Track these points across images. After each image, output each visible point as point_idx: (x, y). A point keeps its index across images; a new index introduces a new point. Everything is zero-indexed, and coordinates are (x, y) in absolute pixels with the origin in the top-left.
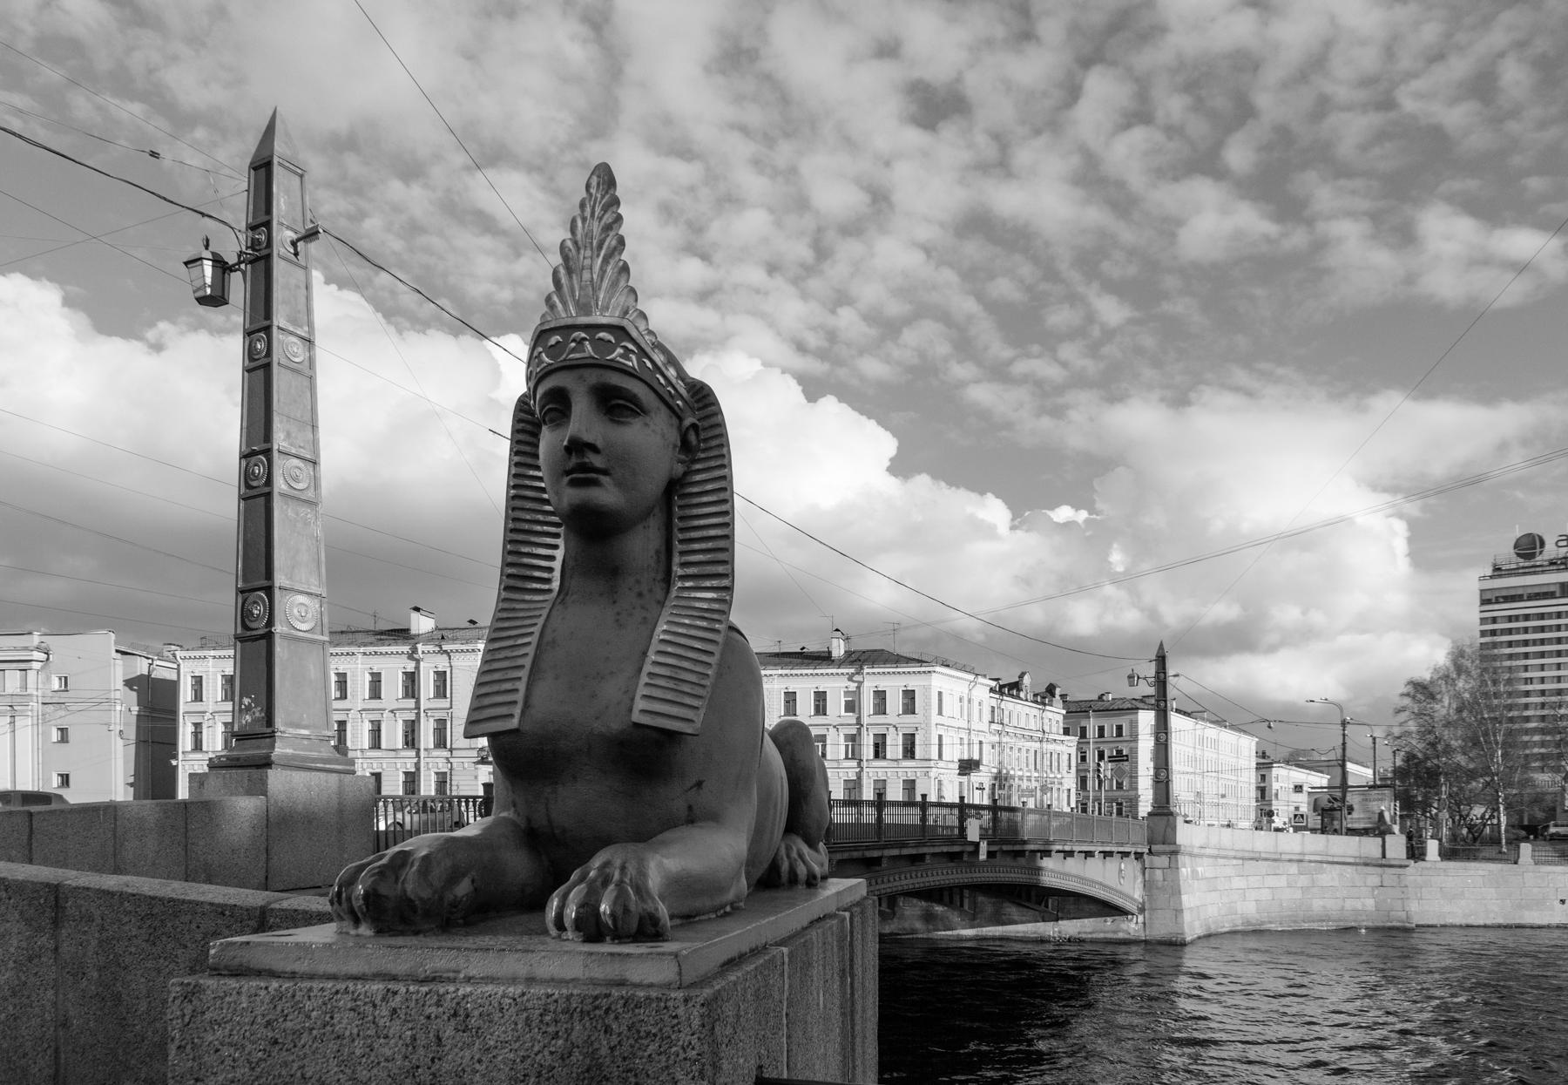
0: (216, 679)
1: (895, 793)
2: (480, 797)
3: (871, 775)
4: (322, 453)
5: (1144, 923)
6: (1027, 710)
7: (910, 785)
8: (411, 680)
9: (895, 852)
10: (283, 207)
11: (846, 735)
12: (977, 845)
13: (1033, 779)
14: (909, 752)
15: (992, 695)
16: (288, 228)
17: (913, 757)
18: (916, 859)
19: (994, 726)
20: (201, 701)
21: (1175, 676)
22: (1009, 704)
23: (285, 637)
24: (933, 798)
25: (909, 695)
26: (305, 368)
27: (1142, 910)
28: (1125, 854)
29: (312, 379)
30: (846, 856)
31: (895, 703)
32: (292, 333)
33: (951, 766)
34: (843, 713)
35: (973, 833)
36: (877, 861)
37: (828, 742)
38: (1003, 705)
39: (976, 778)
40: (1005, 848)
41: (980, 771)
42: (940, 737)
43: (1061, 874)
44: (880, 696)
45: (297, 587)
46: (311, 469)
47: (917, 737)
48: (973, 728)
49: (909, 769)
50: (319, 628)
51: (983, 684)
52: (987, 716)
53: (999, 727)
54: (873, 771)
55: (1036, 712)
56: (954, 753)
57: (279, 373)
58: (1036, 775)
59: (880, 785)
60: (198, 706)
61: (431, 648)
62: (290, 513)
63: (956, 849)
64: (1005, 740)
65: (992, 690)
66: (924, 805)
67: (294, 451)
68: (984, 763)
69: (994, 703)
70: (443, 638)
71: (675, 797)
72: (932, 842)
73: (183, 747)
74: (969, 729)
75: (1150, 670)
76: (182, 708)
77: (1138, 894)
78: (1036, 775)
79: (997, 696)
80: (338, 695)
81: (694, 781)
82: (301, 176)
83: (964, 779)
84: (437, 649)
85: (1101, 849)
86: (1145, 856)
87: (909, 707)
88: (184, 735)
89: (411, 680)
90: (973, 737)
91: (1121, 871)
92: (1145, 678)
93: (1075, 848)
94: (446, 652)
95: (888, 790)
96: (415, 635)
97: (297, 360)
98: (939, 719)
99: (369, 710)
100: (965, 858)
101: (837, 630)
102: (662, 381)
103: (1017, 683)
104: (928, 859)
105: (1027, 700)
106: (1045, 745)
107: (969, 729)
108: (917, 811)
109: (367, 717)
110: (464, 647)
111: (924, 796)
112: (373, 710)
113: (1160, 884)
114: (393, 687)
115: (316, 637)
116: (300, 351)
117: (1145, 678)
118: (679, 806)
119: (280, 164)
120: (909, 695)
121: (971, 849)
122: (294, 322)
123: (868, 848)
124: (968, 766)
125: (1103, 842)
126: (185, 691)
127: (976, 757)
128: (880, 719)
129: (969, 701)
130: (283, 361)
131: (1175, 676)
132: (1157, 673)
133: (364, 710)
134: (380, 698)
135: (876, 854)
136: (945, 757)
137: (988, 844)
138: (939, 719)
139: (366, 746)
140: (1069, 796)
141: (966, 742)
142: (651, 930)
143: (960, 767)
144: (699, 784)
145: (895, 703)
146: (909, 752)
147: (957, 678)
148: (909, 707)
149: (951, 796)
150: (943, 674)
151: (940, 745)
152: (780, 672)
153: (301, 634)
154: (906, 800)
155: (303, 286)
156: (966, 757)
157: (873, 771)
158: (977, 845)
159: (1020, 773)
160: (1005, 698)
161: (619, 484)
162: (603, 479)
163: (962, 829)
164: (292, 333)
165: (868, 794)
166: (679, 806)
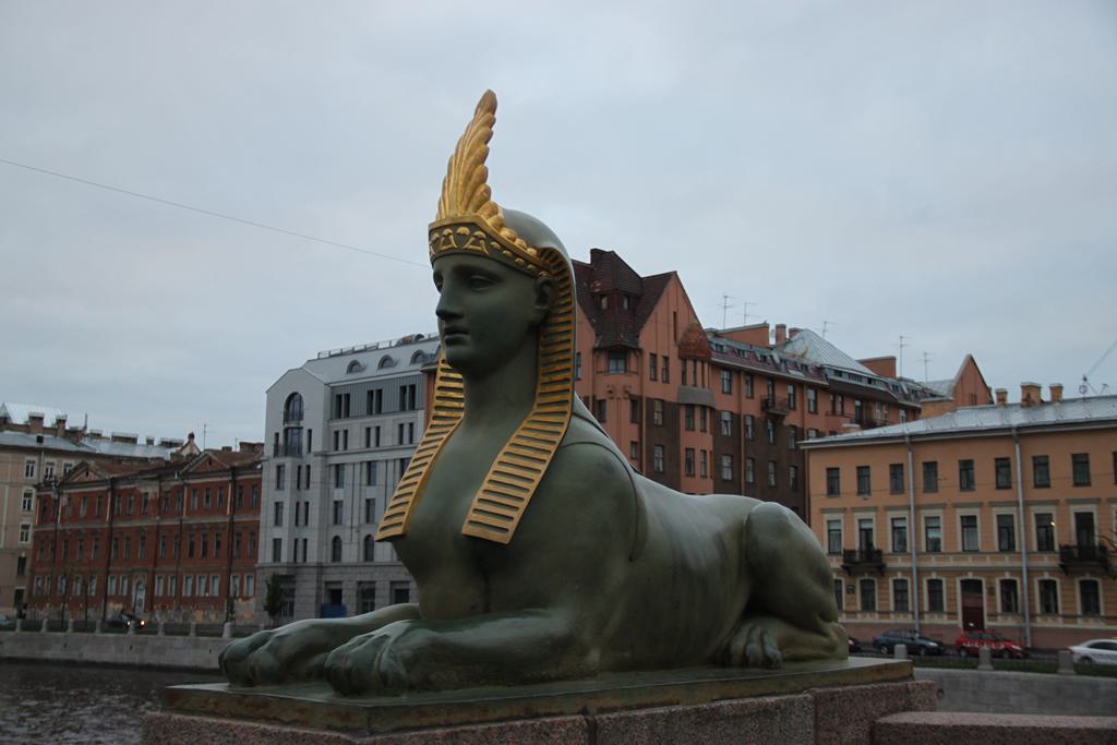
60: (834, 502)
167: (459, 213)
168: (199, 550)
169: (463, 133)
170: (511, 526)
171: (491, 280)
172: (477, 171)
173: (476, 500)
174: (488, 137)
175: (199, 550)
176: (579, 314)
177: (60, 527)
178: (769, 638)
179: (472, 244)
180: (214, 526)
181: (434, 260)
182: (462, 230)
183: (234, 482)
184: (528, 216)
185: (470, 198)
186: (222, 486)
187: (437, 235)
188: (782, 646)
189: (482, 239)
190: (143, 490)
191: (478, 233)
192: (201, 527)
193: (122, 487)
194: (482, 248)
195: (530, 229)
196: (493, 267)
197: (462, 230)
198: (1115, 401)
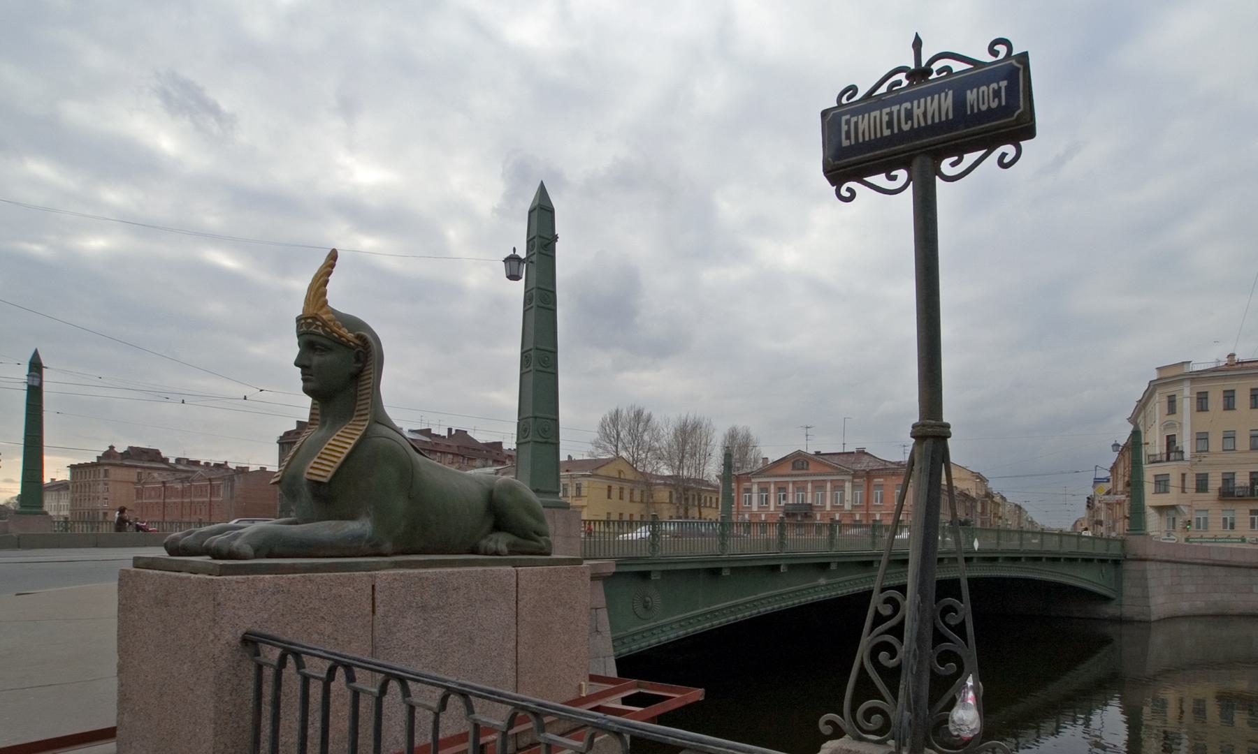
156: (1194, 490)
167: (312, 311)
168: (198, 511)
169: (1126, 441)
170: (330, 475)
171: (326, 349)
172: (321, 290)
173: (312, 462)
174: (329, 273)
175: (198, 511)
176: (469, 472)
177: (144, 501)
179: (315, 328)
180: (203, 502)
181: (298, 337)
182: (309, 321)
183: (211, 484)
184: (359, 319)
185: (316, 304)
186: (206, 486)
187: (303, 321)
189: (320, 326)
190: (176, 487)
191: (318, 323)
192: (198, 502)
193: (168, 485)
194: (320, 331)
195: (354, 324)
196: (325, 342)
197: (309, 321)
198: (1254, 572)
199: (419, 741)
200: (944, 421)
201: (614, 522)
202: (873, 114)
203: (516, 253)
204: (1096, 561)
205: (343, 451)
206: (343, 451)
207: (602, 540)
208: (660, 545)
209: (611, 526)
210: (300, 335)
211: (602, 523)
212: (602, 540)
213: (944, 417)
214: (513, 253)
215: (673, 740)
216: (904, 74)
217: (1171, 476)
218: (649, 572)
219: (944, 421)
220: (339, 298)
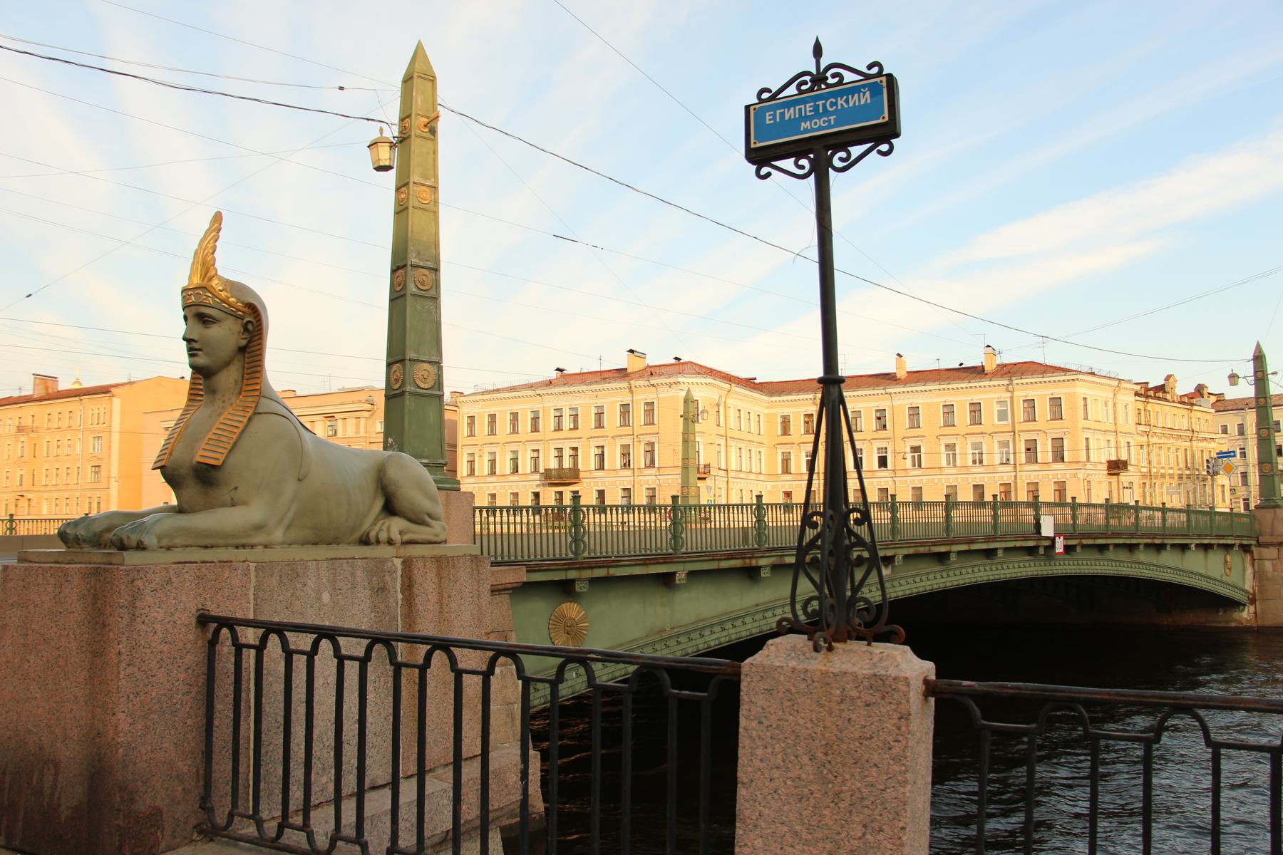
0: (463, 419)
1: (966, 495)
2: (669, 506)
3: (1024, 478)
4: (442, 263)
5: (1255, 613)
6: (1175, 411)
7: (1061, 489)
8: (625, 409)
9: (964, 547)
10: (420, 103)
11: (972, 444)
12: (1053, 540)
13: (1184, 476)
14: (1059, 457)
15: (1137, 398)
16: (422, 116)
17: (1062, 459)
18: (990, 553)
19: (1141, 428)
20: (518, 433)
21: (1273, 374)
22: (1155, 406)
23: (411, 394)
24: (1082, 499)
25: (1056, 402)
26: (431, 207)
27: (1253, 601)
28: (1228, 547)
29: (436, 213)
30: (911, 551)
31: (1043, 410)
32: (423, 185)
33: (1099, 467)
34: (996, 421)
35: (1047, 529)
36: (947, 554)
37: (958, 451)
38: (1149, 407)
39: (1125, 478)
40: (1085, 542)
41: (1128, 471)
42: (1087, 439)
43: (1180, 570)
44: (1030, 403)
45: (422, 358)
46: (434, 275)
47: (1065, 441)
48: (1119, 430)
49: (1059, 472)
50: (436, 386)
51: (1127, 389)
52: (1132, 419)
53: (1147, 429)
54: (1029, 473)
55: (1186, 413)
56: (1102, 455)
57: (413, 213)
58: (1188, 472)
59: (950, 491)
60: (471, 440)
61: (642, 382)
62: (419, 307)
63: (1031, 544)
64: (1153, 440)
65: (1137, 394)
66: (1074, 506)
67: (421, 264)
68: (1133, 463)
69: (1140, 406)
70: (652, 374)
71: (224, 494)
72: (1003, 539)
73: (462, 473)
74: (1116, 432)
75: (1248, 370)
76: (460, 442)
77: (1249, 585)
78: (1188, 472)
79: (1143, 399)
80: (572, 426)
81: (233, 487)
82: (433, 81)
83: (1114, 479)
84: (647, 383)
85: (1198, 541)
86: (1253, 548)
87: (1057, 415)
88: (462, 464)
89: (625, 409)
90: (1120, 439)
91: (1226, 562)
92: (1245, 377)
93: (1166, 541)
94: (653, 385)
95: (1040, 493)
96: (631, 373)
97: (426, 202)
98: (1086, 424)
99: (594, 437)
100: (1042, 551)
101: (988, 346)
102: (226, 306)
103: (1163, 385)
104: (1000, 553)
105: (1174, 402)
106: (1195, 444)
107: (1116, 432)
108: (1068, 511)
109: (487, 449)
110: (667, 381)
111: (1074, 498)
112: (598, 437)
113: (1270, 575)
114: (612, 418)
115: (435, 392)
116: (428, 196)
117: (1245, 377)
118: (227, 498)
119: (419, 77)
120: (1056, 402)
121: (1047, 543)
122: (425, 177)
123: (935, 544)
124: (1116, 467)
125: (1200, 535)
126: (463, 429)
127: (1123, 458)
128: (1031, 425)
129: (1115, 404)
130: (417, 204)
131: (1273, 374)
132: (1255, 372)
133: (591, 438)
134: (603, 427)
135: (943, 549)
136: (1092, 460)
137: (1064, 539)
138: (1086, 424)
139: (593, 468)
140: (1223, 492)
141: (1113, 444)
142: (141, 546)
143: (1109, 468)
144: (236, 488)
145: (1043, 410)
146: (1059, 457)
147: (1101, 384)
148: (1057, 415)
149: (1098, 498)
150: (1087, 381)
151: (1088, 449)
152: (938, 387)
153: (424, 391)
154: (1057, 501)
155: (432, 152)
156: (1113, 458)
157: (1029, 473)
158: (1053, 540)
159: (1171, 472)
160: (1151, 400)
161: (207, 354)
162: (199, 353)
163: (1038, 526)
164: (423, 185)
165: (1023, 496)
166: (227, 498)
178: (396, 526)
188: (401, 533)
199: (402, 844)
200: (840, 374)
201: (501, 508)
202: (797, 108)
203: (384, 135)
204: (1142, 547)
205: (235, 430)
206: (235, 430)
207: (637, 529)
208: (587, 541)
209: (498, 514)
210: (186, 307)
211: (484, 510)
212: (637, 529)
213: (840, 366)
214: (379, 135)
215: (1166, 689)
216: (828, 81)
217: (102, 468)
218: (572, 581)
219: (840, 374)
220: (230, 267)
